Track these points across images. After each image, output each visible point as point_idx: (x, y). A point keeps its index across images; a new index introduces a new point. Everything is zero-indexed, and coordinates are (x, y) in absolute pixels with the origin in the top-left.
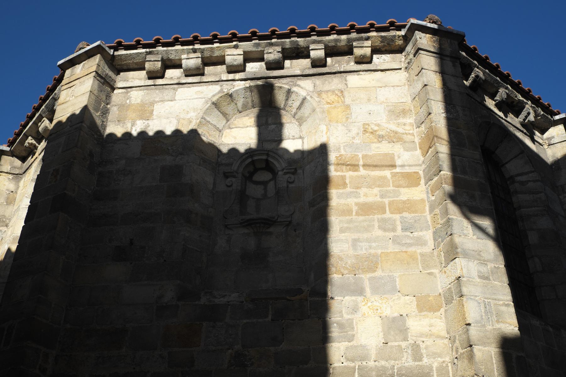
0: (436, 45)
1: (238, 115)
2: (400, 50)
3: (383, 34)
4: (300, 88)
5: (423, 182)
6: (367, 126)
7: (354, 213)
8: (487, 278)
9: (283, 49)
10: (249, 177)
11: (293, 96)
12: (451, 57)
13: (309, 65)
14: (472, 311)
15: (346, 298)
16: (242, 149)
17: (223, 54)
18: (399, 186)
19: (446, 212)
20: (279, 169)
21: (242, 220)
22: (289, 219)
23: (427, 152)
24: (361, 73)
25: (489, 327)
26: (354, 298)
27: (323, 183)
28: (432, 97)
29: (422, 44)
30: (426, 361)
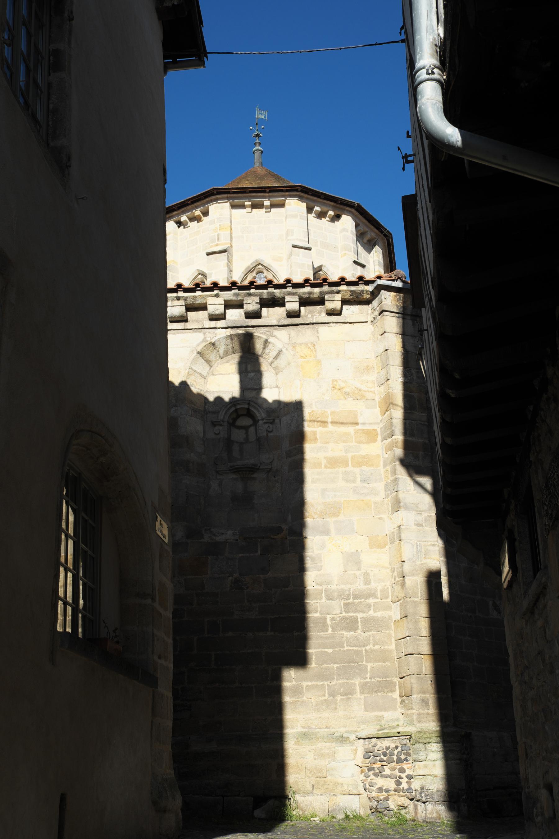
0: (400, 305)
1: (220, 360)
2: (368, 302)
3: (353, 288)
4: (276, 339)
5: (379, 438)
6: (335, 383)
7: (323, 466)
8: (421, 525)
9: (261, 299)
10: (232, 424)
11: (270, 346)
12: (412, 315)
13: (285, 315)
14: (407, 552)
15: (317, 537)
16: (227, 398)
17: (205, 302)
18: (360, 442)
19: (394, 472)
20: (260, 418)
21: (231, 467)
22: (270, 467)
23: (385, 414)
24: (331, 324)
25: (418, 563)
26: (322, 537)
27: (298, 438)
28: (391, 363)
29: (386, 305)
30: (373, 585)
